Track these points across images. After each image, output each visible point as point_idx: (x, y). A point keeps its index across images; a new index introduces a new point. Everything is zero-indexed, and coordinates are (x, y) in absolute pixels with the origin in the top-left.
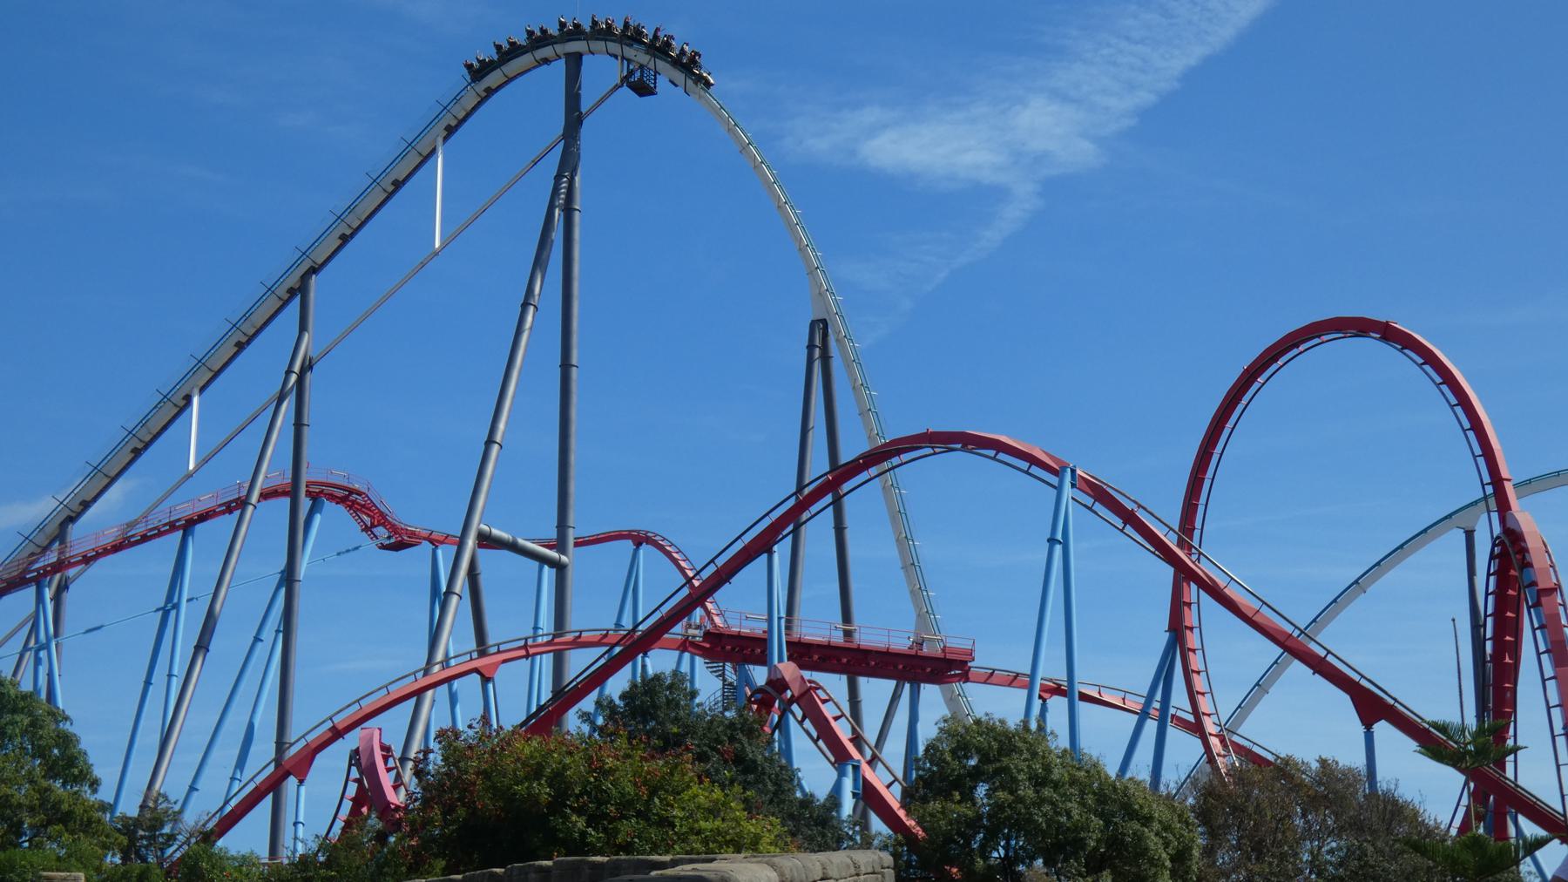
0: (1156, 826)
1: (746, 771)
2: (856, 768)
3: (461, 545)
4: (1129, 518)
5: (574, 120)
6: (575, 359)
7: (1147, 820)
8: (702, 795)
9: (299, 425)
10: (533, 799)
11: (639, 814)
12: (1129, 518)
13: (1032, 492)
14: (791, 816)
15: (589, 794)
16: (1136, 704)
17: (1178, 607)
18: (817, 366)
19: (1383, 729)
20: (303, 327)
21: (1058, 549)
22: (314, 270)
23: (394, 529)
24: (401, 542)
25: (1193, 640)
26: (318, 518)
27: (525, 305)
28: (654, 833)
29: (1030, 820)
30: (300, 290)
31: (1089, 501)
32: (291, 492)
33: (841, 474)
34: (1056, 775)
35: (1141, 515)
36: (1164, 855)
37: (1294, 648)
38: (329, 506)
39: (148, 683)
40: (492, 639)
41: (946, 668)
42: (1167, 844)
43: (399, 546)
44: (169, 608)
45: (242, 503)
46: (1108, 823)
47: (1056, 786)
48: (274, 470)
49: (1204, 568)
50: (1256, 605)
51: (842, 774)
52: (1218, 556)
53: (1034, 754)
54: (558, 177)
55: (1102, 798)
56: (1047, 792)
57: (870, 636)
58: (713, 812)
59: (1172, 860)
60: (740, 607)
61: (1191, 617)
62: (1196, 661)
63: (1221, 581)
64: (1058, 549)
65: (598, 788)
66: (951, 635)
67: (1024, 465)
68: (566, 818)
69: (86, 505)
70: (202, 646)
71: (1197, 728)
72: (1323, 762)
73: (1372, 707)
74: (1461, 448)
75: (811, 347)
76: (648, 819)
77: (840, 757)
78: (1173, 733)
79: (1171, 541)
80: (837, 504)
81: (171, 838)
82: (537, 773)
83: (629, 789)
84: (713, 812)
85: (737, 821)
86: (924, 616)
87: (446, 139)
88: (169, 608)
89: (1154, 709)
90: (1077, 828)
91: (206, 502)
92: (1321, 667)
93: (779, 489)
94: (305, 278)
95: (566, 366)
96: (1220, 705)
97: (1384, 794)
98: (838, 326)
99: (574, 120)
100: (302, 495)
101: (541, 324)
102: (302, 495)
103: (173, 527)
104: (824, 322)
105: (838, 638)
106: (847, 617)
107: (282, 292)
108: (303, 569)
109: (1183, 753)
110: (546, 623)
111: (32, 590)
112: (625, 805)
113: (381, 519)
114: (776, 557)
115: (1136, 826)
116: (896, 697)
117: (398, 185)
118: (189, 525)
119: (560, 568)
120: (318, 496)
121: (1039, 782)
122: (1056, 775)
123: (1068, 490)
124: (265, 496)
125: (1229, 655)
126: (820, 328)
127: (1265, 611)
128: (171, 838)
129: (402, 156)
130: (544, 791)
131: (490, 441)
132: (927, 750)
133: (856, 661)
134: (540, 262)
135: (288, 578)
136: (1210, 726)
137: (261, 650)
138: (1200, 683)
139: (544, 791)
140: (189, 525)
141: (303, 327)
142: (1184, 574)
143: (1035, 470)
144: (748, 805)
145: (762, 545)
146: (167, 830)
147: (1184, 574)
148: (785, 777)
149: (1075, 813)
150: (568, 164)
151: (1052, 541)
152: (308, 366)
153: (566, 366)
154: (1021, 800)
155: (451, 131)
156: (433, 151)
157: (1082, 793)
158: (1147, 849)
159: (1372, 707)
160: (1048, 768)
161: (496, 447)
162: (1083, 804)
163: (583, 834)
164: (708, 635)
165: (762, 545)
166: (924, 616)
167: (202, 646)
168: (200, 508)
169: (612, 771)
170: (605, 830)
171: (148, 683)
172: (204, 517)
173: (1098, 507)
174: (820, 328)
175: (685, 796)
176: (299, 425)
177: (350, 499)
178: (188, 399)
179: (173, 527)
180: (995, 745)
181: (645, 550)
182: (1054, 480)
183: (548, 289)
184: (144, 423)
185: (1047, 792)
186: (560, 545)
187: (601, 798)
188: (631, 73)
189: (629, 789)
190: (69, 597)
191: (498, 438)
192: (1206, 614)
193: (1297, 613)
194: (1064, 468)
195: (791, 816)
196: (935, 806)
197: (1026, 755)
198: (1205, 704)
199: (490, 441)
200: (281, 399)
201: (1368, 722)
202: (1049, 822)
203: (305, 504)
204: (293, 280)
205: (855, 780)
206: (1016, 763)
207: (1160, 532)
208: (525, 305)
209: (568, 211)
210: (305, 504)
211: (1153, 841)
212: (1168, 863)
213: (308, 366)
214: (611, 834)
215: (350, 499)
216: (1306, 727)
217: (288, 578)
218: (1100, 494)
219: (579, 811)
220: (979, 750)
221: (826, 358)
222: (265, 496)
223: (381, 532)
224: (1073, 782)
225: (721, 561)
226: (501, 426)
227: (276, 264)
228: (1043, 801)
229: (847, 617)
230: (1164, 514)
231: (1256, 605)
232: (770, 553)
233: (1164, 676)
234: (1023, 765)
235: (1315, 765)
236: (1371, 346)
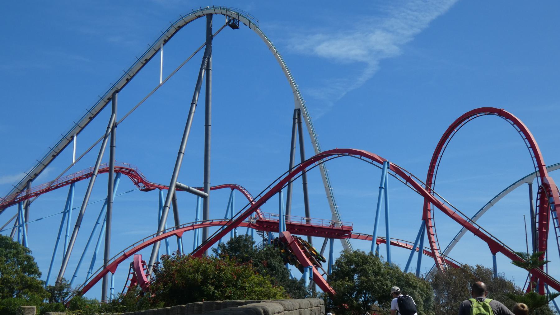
0: (418, 289)
1: (272, 270)
2: (311, 269)
3: (170, 189)
4: (408, 180)
8: (256, 278)
9: (112, 147)
11: (233, 285)
12: (408, 180)
13: (374, 171)
14: (288, 286)
15: (215, 278)
16: (411, 246)
17: (426, 211)
18: (297, 126)
19: (499, 255)
20: (113, 112)
21: (383, 191)
22: (117, 91)
23: (146, 184)
24: (148, 188)
25: (431, 223)
26: (119, 180)
27: (192, 104)
28: (239, 292)
30: (112, 99)
31: (394, 173)
32: (109, 170)
33: (305, 164)
35: (412, 178)
36: (421, 300)
37: (467, 226)
38: (122, 175)
39: (58, 238)
40: (181, 223)
41: (343, 233)
42: (422, 296)
43: (147, 190)
44: (66, 212)
45: (92, 175)
47: (383, 275)
48: (103, 163)
49: (435, 197)
50: (454, 210)
52: (440, 193)
53: (375, 264)
54: (204, 58)
56: (379, 277)
57: (315, 222)
58: (260, 285)
59: (424, 302)
61: (430, 215)
62: (432, 231)
63: (441, 202)
64: (383, 191)
66: (345, 221)
67: (371, 161)
68: (207, 287)
69: (36, 175)
70: (78, 225)
72: (478, 267)
73: (495, 247)
74: (527, 155)
75: (294, 119)
76: (236, 287)
78: (424, 256)
79: (423, 188)
80: (304, 175)
81: (67, 294)
82: (197, 271)
83: (230, 276)
84: (260, 285)
85: (268, 288)
86: (335, 215)
87: (164, 45)
88: (66, 212)
89: (417, 248)
94: (114, 94)
95: (207, 125)
96: (441, 246)
97: (500, 278)
98: (304, 111)
100: (113, 172)
101: (198, 111)
102: (113, 172)
103: (67, 183)
104: (299, 110)
105: (304, 223)
106: (307, 215)
107: (106, 99)
109: (428, 263)
110: (200, 217)
112: (229, 282)
113: (141, 180)
114: (282, 194)
116: (325, 244)
117: (147, 61)
118: (73, 182)
119: (205, 198)
120: (119, 172)
121: (376, 274)
122: (383, 271)
123: (386, 170)
124: (100, 172)
125: (444, 228)
126: (298, 112)
127: (457, 213)
128: (67, 294)
129: (149, 50)
130: (199, 277)
131: (180, 153)
132: (336, 262)
134: (197, 88)
135: (108, 201)
136: (437, 254)
138: (434, 238)
139: (199, 277)
140: (73, 182)
141: (113, 112)
142: (428, 200)
143: (374, 162)
144: (273, 282)
145: (277, 189)
146: (65, 291)
147: (428, 200)
150: (208, 54)
151: (381, 188)
152: (115, 126)
153: (207, 125)
154: (370, 280)
155: (166, 42)
156: (160, 49)
157: (392, 277)
159: (495, 247)
160: (380, 269)
161: (182, 155)
163: (213, 292)
164: (258, 222)
165: (277, 189)
166: (335, 215)
167: (78, 225)
168: (77, 176)
169: (223, 270)
170: (221, 291)
171: (58, 238)
172: (78, 179)
173: (397, 176)
174: (298, 112)
175: (250, 279)
176: (112, 147)
177: (130, 173)
178: (72, 138)
179: (67, 183)
181: (235, 191)
182: (381, 166)
183: (200, 98)
184: (57, 146)
186: (205, 190)
187: (220, 279)
188: (230, 21)
189: (230, 276)
190: (30, 208)
192: (436, 214)
193: (468, 213)
194: (385, 162)
196: (339, 282)
197: (372, 264)
198: (435, 246)
199: (180, 153)
202: (380, 288)
203: (114, 175)
204: (110, 95)
205: (310, 273)
206: (368, 267)
208: (192, 104)
209: (208, 70)
210: (114, 175)
212: (422, 303)
213: (115, 126)
214: (223, 292)
215: (130, 173)
216: (472, 254)
217: (108, 201)
218: (398, 171)
219: (212, 284)
221: (300, 123)
222: (100, 172)
223: (141, 185)
225: (262, 195)
226: (184, 147)
227: (104, 89)
228: (377, 280)
229: (307, 215)
230: (421, 178)
231: (454, 210)
232: (280, 192)
233: (421, 236)
234: (371, 268)
235: (475, 268)
236: (495, 118)
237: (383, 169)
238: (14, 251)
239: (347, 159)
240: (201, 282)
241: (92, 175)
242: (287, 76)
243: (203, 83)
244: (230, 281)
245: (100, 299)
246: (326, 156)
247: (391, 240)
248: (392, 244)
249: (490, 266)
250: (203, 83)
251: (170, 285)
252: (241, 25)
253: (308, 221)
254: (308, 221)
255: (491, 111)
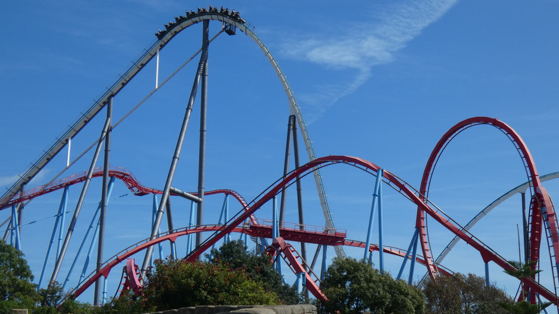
0: (410, 297)
2: (304, 275)
3: (164, 194)
4: (402, 187)
5: (206, 43)
6: (205, 129)
7: (406, 295)
8: (249, 284)
9: (106, 151)
10: (188, 285)
11: (226, 291)
12: (402, 187)
13: (368, 178)
14: (281, 292)
15: (208, 283)
16: (404, 253)
17: (419, 219)
18: (291, 132)
20: (108, 116)
21: (377, 198)
22: (112, 96)
23: (140, 188)
24: (142, 193)
25: (424, 231)
26: (113, 184)
27: (188, 109)
28: (231, 298)
29: (365, 294)
31: (388, 181)
32: (104, 174)
33: (300, 170)
34: (374, 279)
35: (406, 186)
37: (460, 234)
38: (117, 180)
39: (51, 242)
40: (174, 228)
41: (336, 240)
42: (414, 303)
43: (141, 194)
44: (59, 215)
45: (85, 179)
46: (393, 296)
48: (98, 167)
49: (429, 206)
50: (447, 219)
51: (298, 277)
52: (433, 201)
53: (367, 271)
54: (200, 64)
55: (390, 287)
57: (309, 228)
58: (252, 290)
59: (415, 309)
60: (263, 217)
61: (424, 223)
62: (425, 239)
63: (435, 210)
64: (377, 198)
65: (212, 281)
66: (338, 228)
67: (365, 168)
68: (200, 291)
69: (30, 178)
70: (71, 229)
71: (425, 262)
72: (470, 275)
73: (488, 256)
74: (521, 164)
75: (289, 125)
76: (229, 292)
77: (298, 271)
79: (417, 196)
80: (298, 181)
81: (59, 297)
82: (190, 275)
83: (223, 281)
84: (252, 290)
85: (261, 293)
86: (329, 222)
87: (160, 49)
88: (59, 215)
89: (410, 256)
90: (382, 298)
91: (73, 178)
92: (470, 241)
93: (277, 176)
94: (109, 98)
95: (202, 131)
96: (434, 254)
98: (299, 118)
99: (206, 43)
101: (193, 116)
102: (107, 176)
103: (61, 186)
104: (294, 116)
105: (298, 229)
106: (301, 221)
107: (101, 103)
108: (107, 202)
109: (420, 271)
110: (194, 222)
111: (11, 208)
113: (135, 184)
114: (276, 200)
115: (403, 297)
116: (318, 250)
117: (143, 66)
118: (67, 186)
119: (199, 203)
121: (368, 281)
122: (374, 279)
123: (380, 177)
124: (94, 176)
125: (437, 236)
126: (293, 118)
127: (450, 221)
128: (59, 297)
129: (145, 55)
130: (192, 282)
131: (175, 157)
132: (328, 269)
133: (304, 237)
134: (193, 94)
135: (102, 205)
136: (430, 262)
137: (92, 230)
138: (426, 246)
139: (192, 282)
140: (67, 186)
141: (108, 116)
142: (422, 208)
143: (369, 170)
145: (271, 195)
146: (58, 294)
147: (422, 208)
148: (278, 278)
149: (381, 292)
150: (204, 59)
151: (375, 195)
152: (110, 130)
153: (202, 131)
154: (362, 287)
156: (156, 54)
157: (383, 285)
158: (407, 305)
159: (488, 256)
160: (371, 276)
162: (384, 289)
163: (206, 297)
165: (271, 195)
166: (329, 222)
167: (71, 229)
169: (216, 275)
170: (214, 296)
171: (51, 242)
172: (72, 183)
173: (391, 183)
174: (293, 118)
176: (106, 151)
177: (124, 177)
179: (61, 186)
180: (353, 268)
181: (229, 196)
182: (375, 173)
183: (196, 103)
184: (51, 149)
185: (371, 285)
186: (199, 195)
187: (213, 285)
188: (226, 27)
189: (223, 281)
190: (24, 211)
191: (177, 156)
192: (429, 221)
193: (461, 222)
194: (379, 169)
195: (281, 292)
196: (331, 289)
198: (428, 254)
199: (175, 157)
200: (100, 141)
201: (486, 261)
202: (372, 295)
203: (108, 179)
204: (105, 99)
205: (303, 279)
206: (359, 274)
207: (413, 192)
208: (188, 109)
209: (203, 76)
210: (108, 179)
211: (409, 303)
212: (414, 310)
213: (110, 130)
215: (124, 177)
216: (464, 263)
217: (102, 205)
218: (392, 179)
219: (205, 289)
220: (347, 269)
221: (295, 129)
222: (94, 176)
223: (135, 189)
224: (380, 281)
225: (256, 201)
226: (179, 152)
227: (99, 93)
228: (370, 288)
229: (301, 221)
230: (415, 186)
231: (447, 219)
232: (274, 198)
233: (414, 244)
234: (363, 275)
235: (467, 276)
236: (489, 127)
237: (377, 177)
238: (8, 254)
239: (342, 166)
240: (194, 287)
241: (85, 179)
242: (275, 68)
243: (198, 89)
244: (223, 287)
245: (92, 303)
246: (320, 163)
247: (384, 248)
248: (385, 251)
249: (482, 275)
250: (198, 89)
251: (163, 289)
252: (237, 31)
253: (301, 227)
254: (301, 227)
255: (485, 120)
